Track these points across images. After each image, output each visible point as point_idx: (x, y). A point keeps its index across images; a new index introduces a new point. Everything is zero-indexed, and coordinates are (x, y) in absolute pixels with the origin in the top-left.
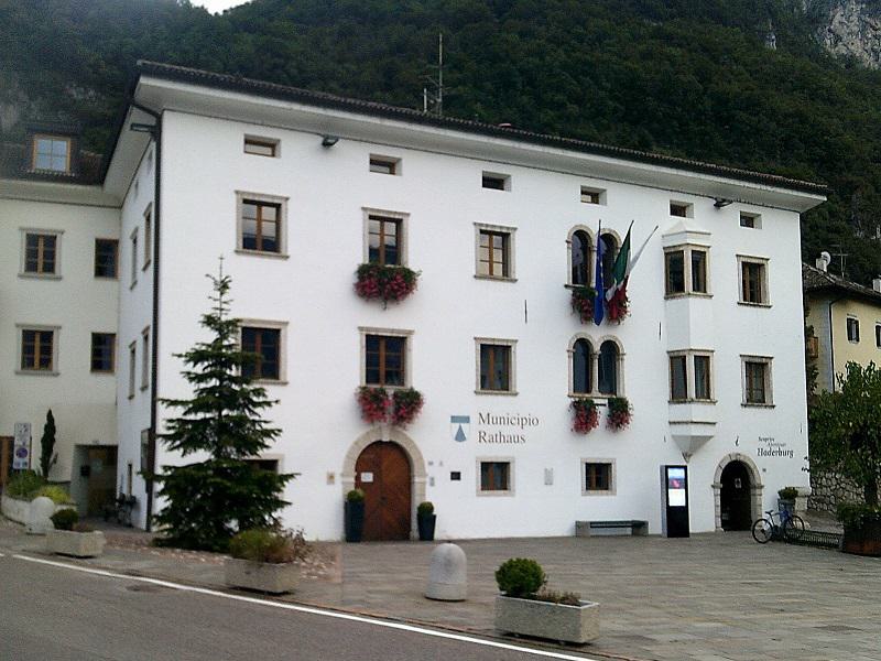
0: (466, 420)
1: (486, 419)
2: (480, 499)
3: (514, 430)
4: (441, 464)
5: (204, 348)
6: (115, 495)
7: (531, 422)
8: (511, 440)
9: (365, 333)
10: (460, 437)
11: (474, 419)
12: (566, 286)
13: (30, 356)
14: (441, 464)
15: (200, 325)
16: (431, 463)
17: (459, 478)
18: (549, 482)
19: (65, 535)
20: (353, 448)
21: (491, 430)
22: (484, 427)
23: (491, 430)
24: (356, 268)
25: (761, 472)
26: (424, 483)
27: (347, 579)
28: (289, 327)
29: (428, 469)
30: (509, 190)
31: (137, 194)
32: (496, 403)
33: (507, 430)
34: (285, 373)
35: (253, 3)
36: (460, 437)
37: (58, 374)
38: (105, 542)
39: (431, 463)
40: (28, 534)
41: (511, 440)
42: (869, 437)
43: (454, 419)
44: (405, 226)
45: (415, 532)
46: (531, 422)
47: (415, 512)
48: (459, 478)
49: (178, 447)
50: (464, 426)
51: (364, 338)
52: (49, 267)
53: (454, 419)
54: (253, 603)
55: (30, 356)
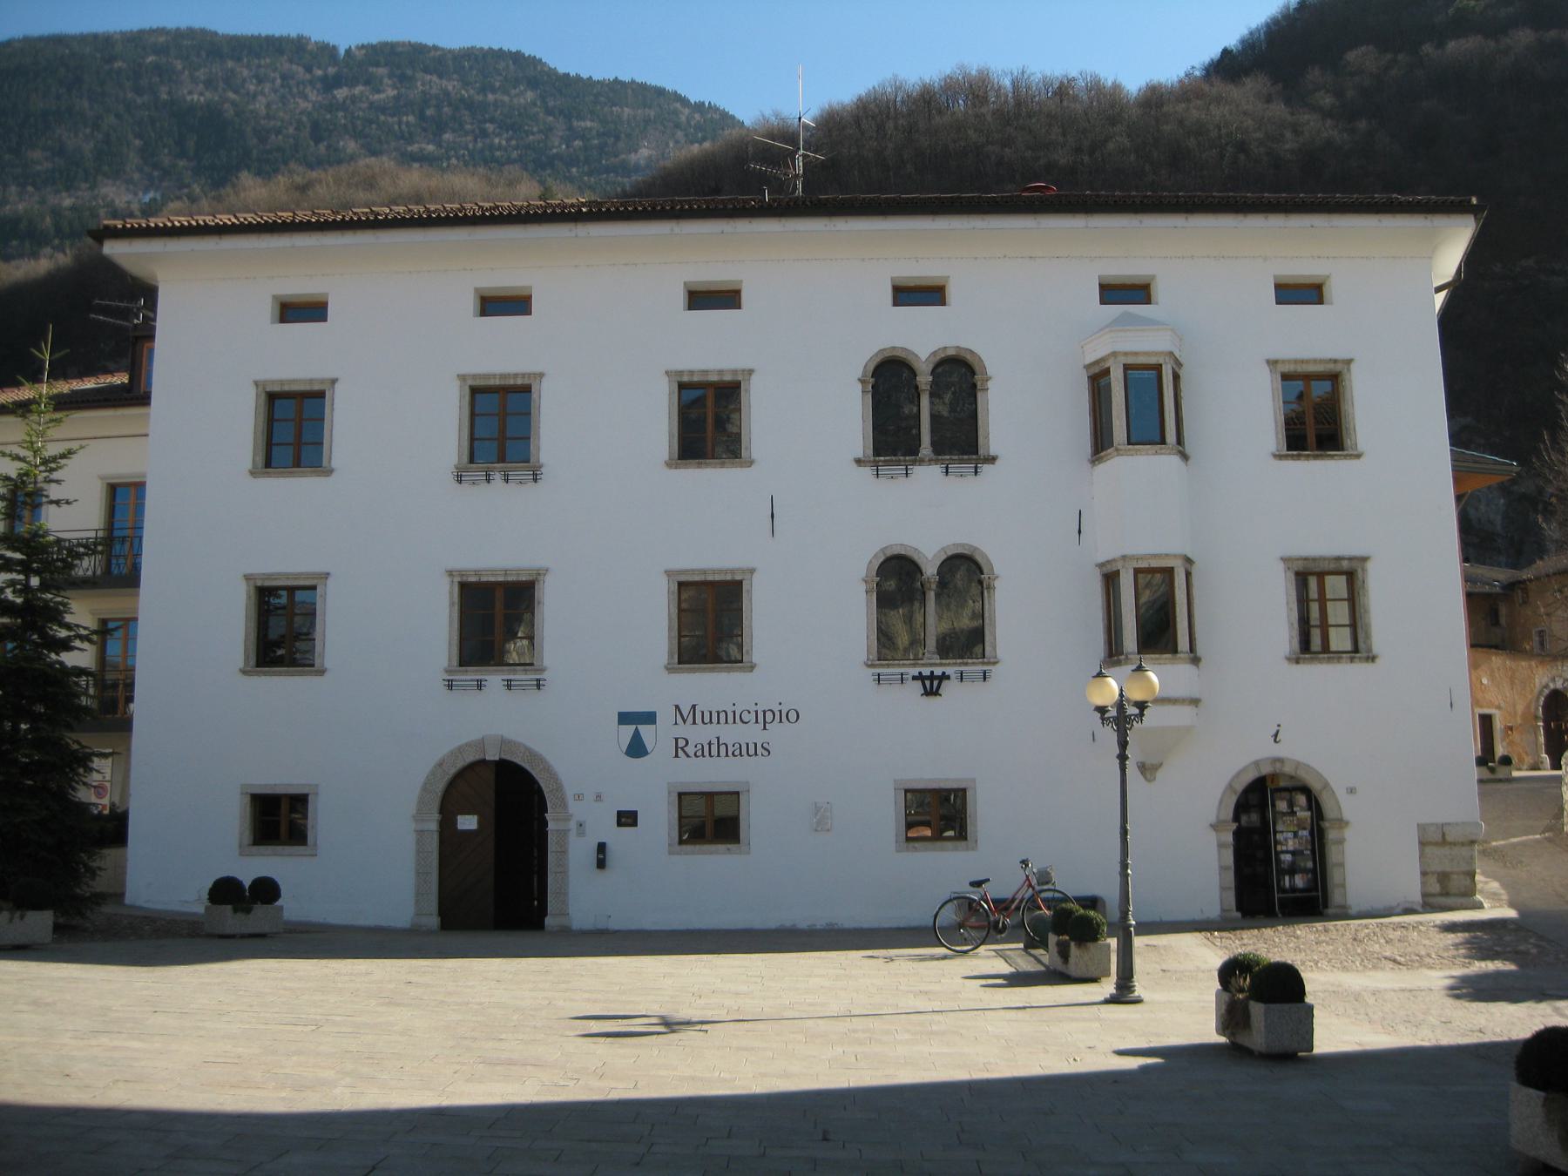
0: (650, 718)
1: (689, 715)
2: (269, 300)
3: (750, 733)
4: (599, 797)
5: (1133, 1063)
6: (1510, 973)
7: (783, 716)
8: (742, 751)
9: (457, 579)
10: (637, 749)
11: (665, 716)
12: (859, 462)
13: (709, 829)
14: (599, 797)
15: (867, 471)
16: (579, 797)
17: (620, 814)
18: (601, 864)
19: (1463, 1035)
20: (433, 773)
21: (699, 734)
22: (683, 730)
23: (699, 734)
24: (210, 885)
25: (1341, 794)
26: (565, 832)
27: (928, 683)
28: (330, 582)
29: (574, 807)
30: (144, 475)
31: (1018, 980)
32: (709, 687)
33: (731, 734)
34: (748, 448)
35: (1301, 7)
36: (637, 749)
37: (751, 463)
38: (246, 178)
39: (579, 797)
40: (1473, 842)
41: (742, 751)
42: (952, 410)
43: (625, 718)
44: (1346, 383)
45: (1117, 376)
46: (783, 716)
47: (1517, 1021)
48: (620, 814)
49: (68, 627)
50: (646, 731)
51: (456, 589)
52: (283, 319)
53: (625, 718)
54: (81, 375)
55: (709, 829)
